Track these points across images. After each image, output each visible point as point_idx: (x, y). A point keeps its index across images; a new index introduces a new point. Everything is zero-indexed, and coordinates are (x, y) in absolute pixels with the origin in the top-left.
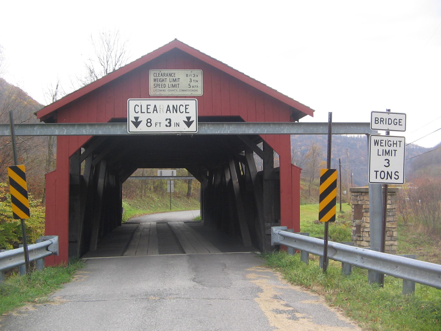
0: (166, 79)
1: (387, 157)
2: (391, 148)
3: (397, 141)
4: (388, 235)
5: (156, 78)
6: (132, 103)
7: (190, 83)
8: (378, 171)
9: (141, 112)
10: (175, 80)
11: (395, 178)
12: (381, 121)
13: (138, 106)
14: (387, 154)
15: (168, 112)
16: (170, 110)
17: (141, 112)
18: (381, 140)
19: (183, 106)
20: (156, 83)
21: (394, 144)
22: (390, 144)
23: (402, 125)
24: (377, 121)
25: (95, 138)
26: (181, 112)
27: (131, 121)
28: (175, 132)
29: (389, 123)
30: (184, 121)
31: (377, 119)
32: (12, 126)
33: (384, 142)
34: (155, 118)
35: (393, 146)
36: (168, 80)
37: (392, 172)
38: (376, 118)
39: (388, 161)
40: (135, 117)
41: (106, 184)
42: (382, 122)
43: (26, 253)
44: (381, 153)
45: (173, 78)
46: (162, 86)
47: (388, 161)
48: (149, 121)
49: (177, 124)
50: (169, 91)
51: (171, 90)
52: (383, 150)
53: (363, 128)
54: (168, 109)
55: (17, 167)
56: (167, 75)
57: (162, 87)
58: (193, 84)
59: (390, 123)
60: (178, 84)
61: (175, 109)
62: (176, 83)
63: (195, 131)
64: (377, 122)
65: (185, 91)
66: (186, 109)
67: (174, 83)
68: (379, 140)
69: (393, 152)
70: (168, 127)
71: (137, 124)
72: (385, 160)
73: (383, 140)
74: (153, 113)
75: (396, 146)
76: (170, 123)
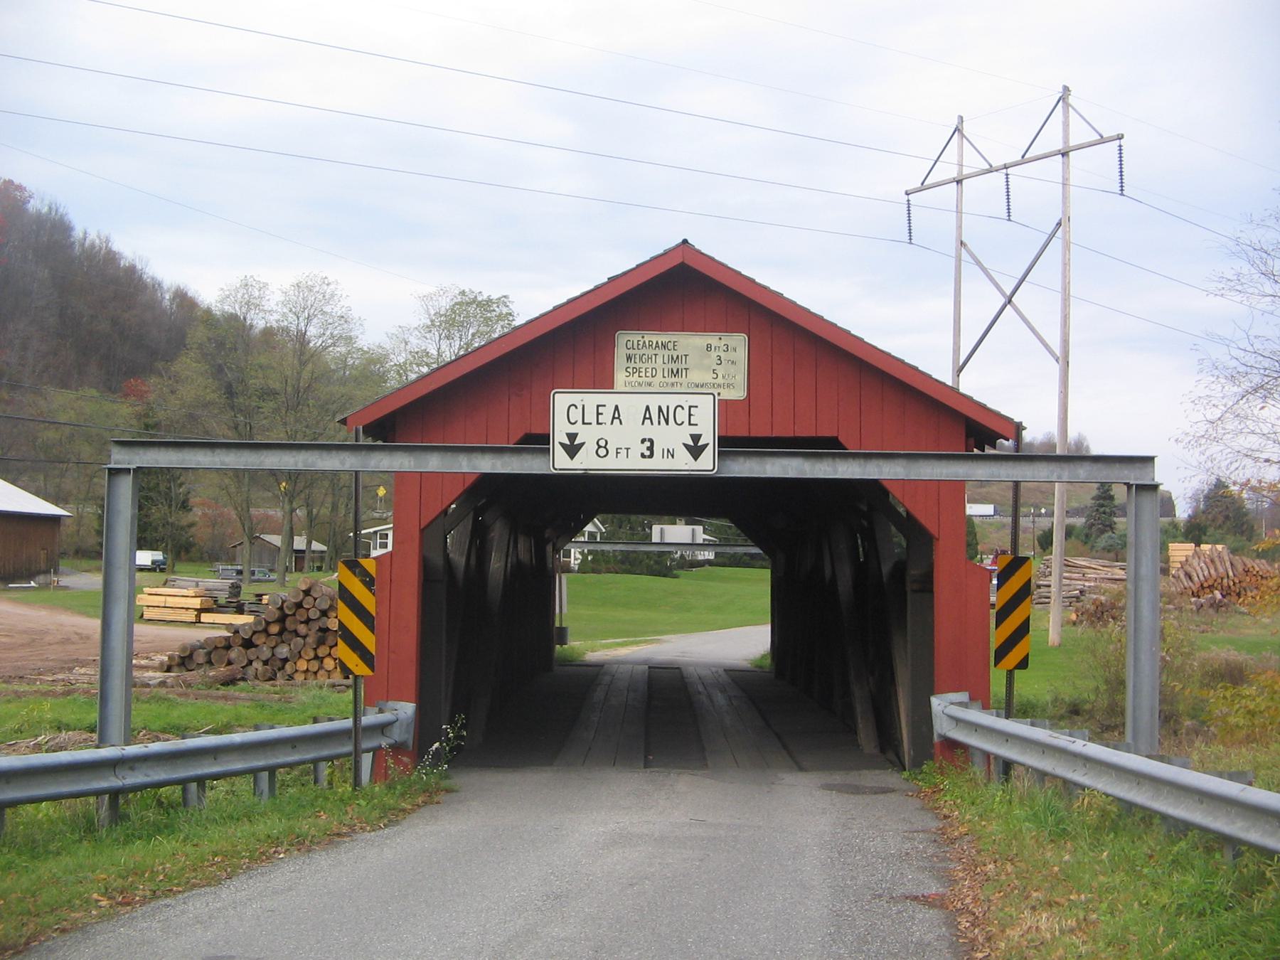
5: (631, 352)
6: (562, 401)
9: (584, 423)
10: (674, 360)
15: (648, 422)
16: (650, 418)
17: (584, 423)
25: (486, 482)
27: (561, 443)
30: (685, 445)
34: (614, 435)
40: (568, 434)
41: (509, 565)
45: (670, 353)
49: (668, 451)
54: (647, 416)
63: (711, 468)
67: (675, 367)
71: (572, 449)
76: (651, 449)
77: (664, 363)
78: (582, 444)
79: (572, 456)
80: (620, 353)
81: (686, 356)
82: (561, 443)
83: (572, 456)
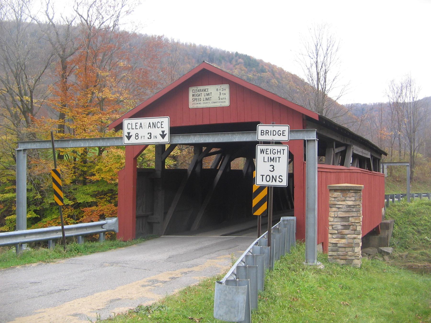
0: (201, 94)
1: (272, 163)
2: (276, 156)
3: (280, 150)
4: (351, 229)
5: (194, 93)
7: (220, 96)
8: (264, 175)
9: (132, 129)
10: (208, 95)
11: (279, 181)
12: (266, 133)
13: (130, 124)
14: (272, 161)
15: (150, 127)
16: (150, 126)
17: (132, 129)
18: (266, 149)
19: (159, 123)
20: (194, 98)
21: (278, 152)
22: (275, 152)
23: (285, 136)
24: (263, 133)
26: (158, 127)
28: (154, 143)
29: (274, 134)
30: (160, 134)
31: (263, 132)
32: (53, 142)
33: (269, 151)
35: (277, 154)
36: (203, 95)
37: (276, 176)
38: (261, 131)
39: (273, 167)
42: (267, 134)
43: (63, 230)
44: (266, 160)
46: (198, 99)
47: (273, 167)
48: (137, 135)
49: (155, 136)
50: (204, 103)
51: (205, 103)
52: (268, 157)
53: (302, 134)
54: (150, 126)
55: (56, 170)
56: (202, 91)
57: (198, 101)
58: (222, 96)
59: (274, 134)
60: (211, 98)
61: (154, 125)
62: (209, 97)
64: (262, 134)
65: (216, 103)
66: (162, 124)
67: (207, 97)
68: (264, 149)
69: (277, 159)
70: (149, 139)
71: (129, 137)
72: (270, 166)
73: (268, 149)
74: (140, 128)
75: (280, 154)
76: (150, 136)
77: (204, 96)
78: (132, 135)
79: (129, 139)
80: (191, 93)
81: (211, 93)
82: (126, 136)
83: (129, 139)
